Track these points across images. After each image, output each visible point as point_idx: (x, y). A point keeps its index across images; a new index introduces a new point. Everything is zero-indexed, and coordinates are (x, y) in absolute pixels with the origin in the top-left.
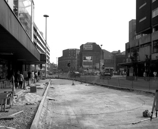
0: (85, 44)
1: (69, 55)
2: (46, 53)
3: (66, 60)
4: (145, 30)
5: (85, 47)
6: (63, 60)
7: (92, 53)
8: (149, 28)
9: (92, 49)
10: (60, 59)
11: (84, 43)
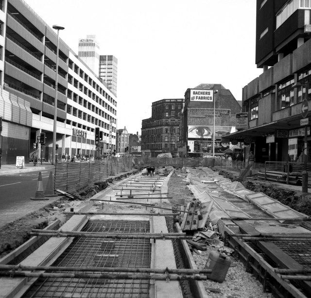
0: (194, 89)
2: (14, 273)
3: (158, 126)
4: (267, 58)
5: (195, 96)
6: (153, 127)
8: (272, 54)
10: (146, 124)
11: (192, 86)
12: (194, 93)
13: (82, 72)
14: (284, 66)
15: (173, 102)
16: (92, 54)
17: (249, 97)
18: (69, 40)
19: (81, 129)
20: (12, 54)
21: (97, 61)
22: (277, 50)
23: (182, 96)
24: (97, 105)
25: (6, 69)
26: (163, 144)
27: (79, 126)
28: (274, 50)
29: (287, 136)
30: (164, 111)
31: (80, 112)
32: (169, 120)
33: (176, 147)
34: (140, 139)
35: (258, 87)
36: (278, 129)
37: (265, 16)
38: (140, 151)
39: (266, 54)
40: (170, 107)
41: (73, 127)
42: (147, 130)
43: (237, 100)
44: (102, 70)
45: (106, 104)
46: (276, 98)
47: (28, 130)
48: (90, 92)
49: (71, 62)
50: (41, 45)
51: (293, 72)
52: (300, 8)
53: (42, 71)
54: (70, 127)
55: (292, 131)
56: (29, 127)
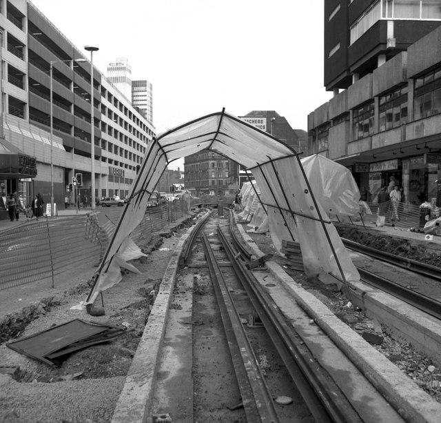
3: (202, 161)
4: (339, 80)
6: (197, 162)
8: (345, 75)
13: (116, 100)
14: (362, 89)
16: (123, 79)
17: (316, 126)
18: (99, 62)
19: (118, 167)
20: (37, 83)
21: (129, 88)
22: (352, 69)
24: (134, 138)
25: (31, 101)
26: (210, 181)
27: (116, 163)
28: (349, 70)
29: (367, 171)
33: (224, 184)
34: (183, 176)
35: (328, 113)
37: (335, 30)
39: (336, 77)
41: (110, 165)
42: (191, 165)
43: (294, 126)
44: (135, 94)
45: (144, 137)
46: (351, 126)
47: (62, 172)
48: (126, 123)
49: (103, 90)
51: (374, 95)
52: (382, 18)
53: (71, 101)
54: (106, 164)
55: (375, 164)
56: (63, 168)
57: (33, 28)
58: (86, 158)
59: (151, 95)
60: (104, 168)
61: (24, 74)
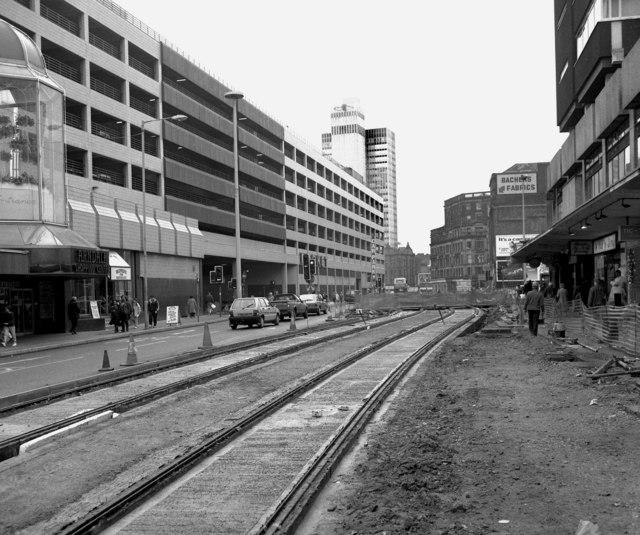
1: (469, 217)
5: (506, 184)
7: (534, 208)
9: (535, 191)
10: (437, 236)
12: (503, 180)
15: (478, 198)
23: (484, 187)
29: (590, 253)
30: (464, 214)
31: (344, 218)
32: (473, 228)
36: (573, 240)
38: (98, 317)
40: (473, 205)
41: (301, 251)
50: (232, 128)
57: (170, 76)
58: (277, 246)
59: (394, 147)
60: (292, 255)
61: (158, 136)
